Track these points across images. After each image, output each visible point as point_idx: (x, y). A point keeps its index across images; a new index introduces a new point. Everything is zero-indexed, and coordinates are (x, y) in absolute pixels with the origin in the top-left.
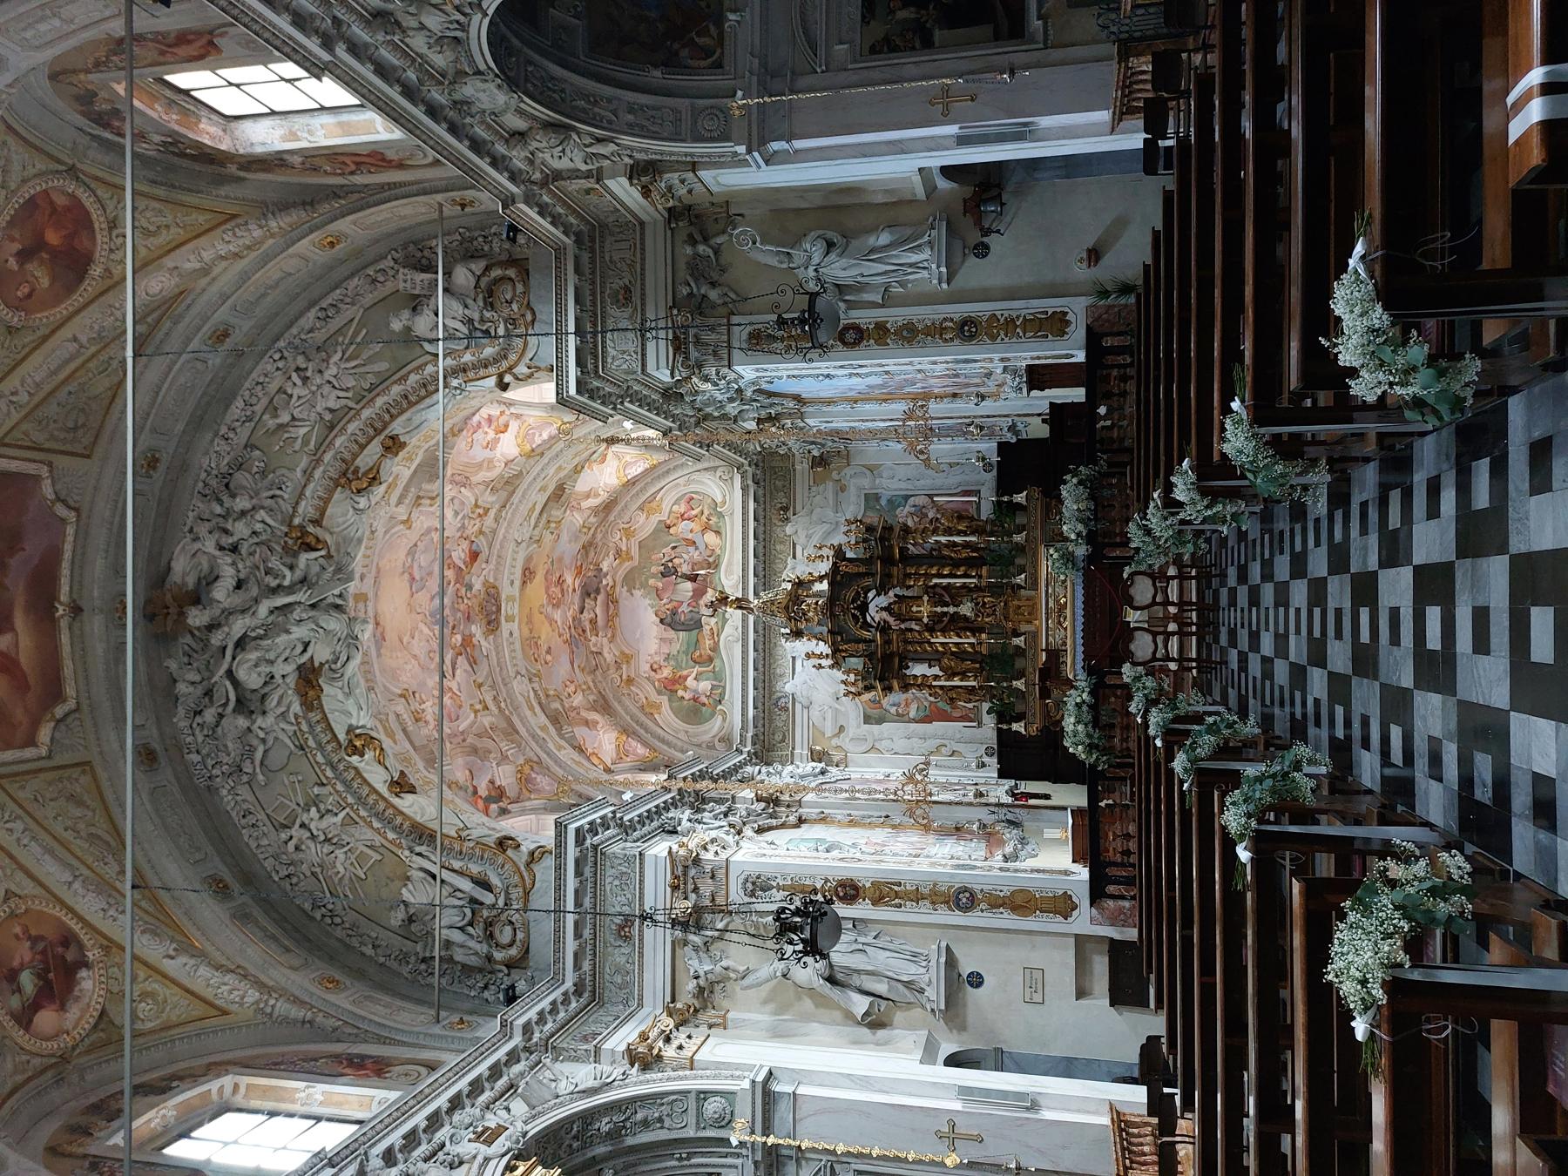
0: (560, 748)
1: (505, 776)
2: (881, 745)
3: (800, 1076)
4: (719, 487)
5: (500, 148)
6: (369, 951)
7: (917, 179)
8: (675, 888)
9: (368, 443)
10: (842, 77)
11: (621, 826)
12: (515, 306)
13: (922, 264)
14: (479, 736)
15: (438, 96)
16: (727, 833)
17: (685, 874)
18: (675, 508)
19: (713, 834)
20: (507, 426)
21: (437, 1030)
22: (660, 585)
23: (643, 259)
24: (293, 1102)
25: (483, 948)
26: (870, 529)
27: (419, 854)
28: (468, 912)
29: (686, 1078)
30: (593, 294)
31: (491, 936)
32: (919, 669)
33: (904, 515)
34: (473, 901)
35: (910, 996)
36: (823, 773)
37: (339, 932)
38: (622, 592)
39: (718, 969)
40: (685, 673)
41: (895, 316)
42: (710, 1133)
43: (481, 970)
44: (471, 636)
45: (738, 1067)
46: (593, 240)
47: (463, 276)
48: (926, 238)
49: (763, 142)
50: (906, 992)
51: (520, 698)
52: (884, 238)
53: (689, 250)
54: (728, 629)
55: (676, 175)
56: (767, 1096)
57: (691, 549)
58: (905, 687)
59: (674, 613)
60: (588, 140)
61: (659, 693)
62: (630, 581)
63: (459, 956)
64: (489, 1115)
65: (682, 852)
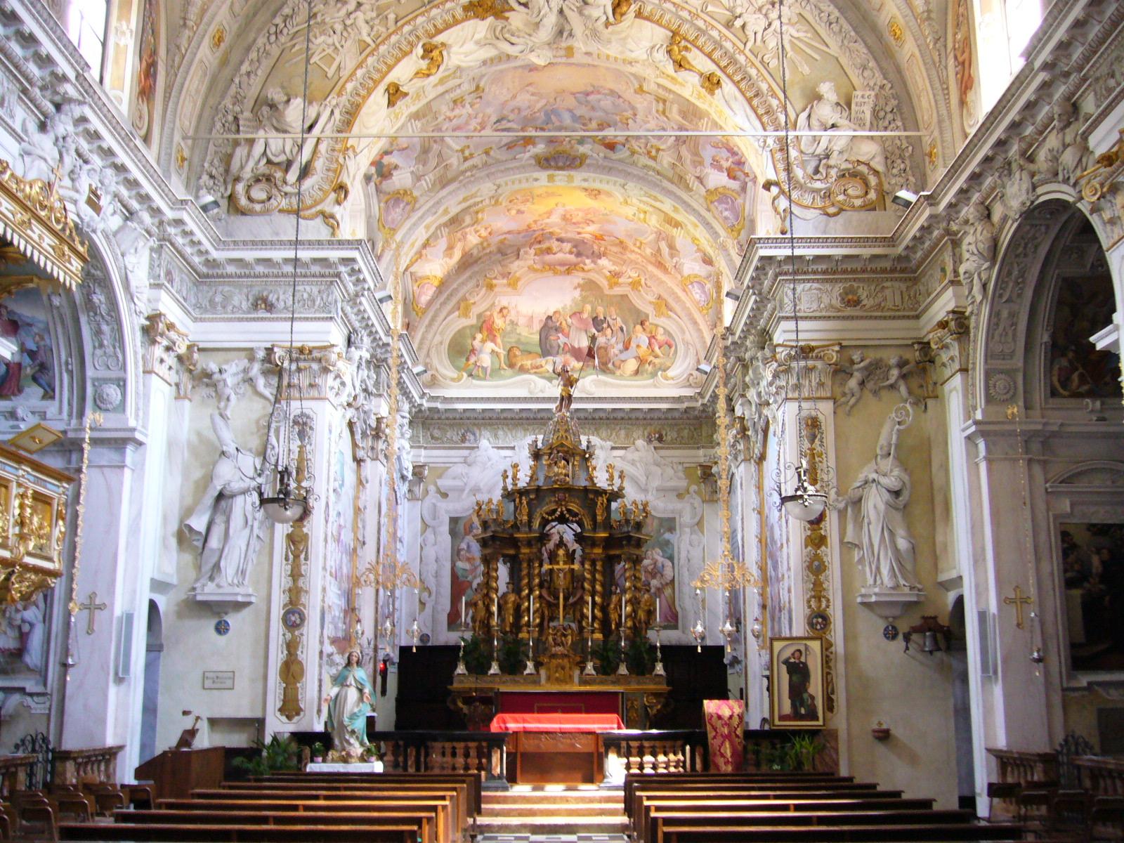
0: (427, 227)
1: (402, 179)
2: (430, 535)
3: (139, 469)
4: (683, 373)
5: (976, 197)
6: (245, 68)
7: (954, 575)
8: (301, 350)
9: (713, 61)
10: (1041, 506)
11: (357, 295)
12: (841, 198)
13: (880, 578)
14: (440, 155)
15: (1014, 149)
16: (349, 395)
17: (313, 360)
18: (661, 331)
19: (349, 383)
20: (734, 178)
21: (177, 138)
22: (585, 316)
23: (885, 318)
24: (119, 19)
25: (247, 174)
26: (639, 526)
27: (332, 112)
28: (282, 158)
29: (136, 367)
30: (854, 271)
31: (258, 181)
32: (503, 571)
33: (654, 556)
34: (289, 164)
35: (207, 568)
36: (403, 478)
37: (261, 41)
38: (577, 278)
39: (228, 391)
40: (499, 340)
41: (832, 554)
42: (90, 390)
43: (227, 171)
44: (534, 144)
45: (146, 414)
46: (903, 271)
47: (869, 151)
48: (902, 582)
49: (984, 434)
50: (210, 565)
51: (474, 190)
52: (902, 544)
53: (893, 361)
54: (542, 383)
55: (957, 354)
56: (120, 442)
57: (620, 346)
58: (487, 560)
59: (558, 329)
60: (984, 277)
61: (479, 316)
62: (590, 287)
63: (240, 152)
64: (109, 198)
65: (334, 357)
